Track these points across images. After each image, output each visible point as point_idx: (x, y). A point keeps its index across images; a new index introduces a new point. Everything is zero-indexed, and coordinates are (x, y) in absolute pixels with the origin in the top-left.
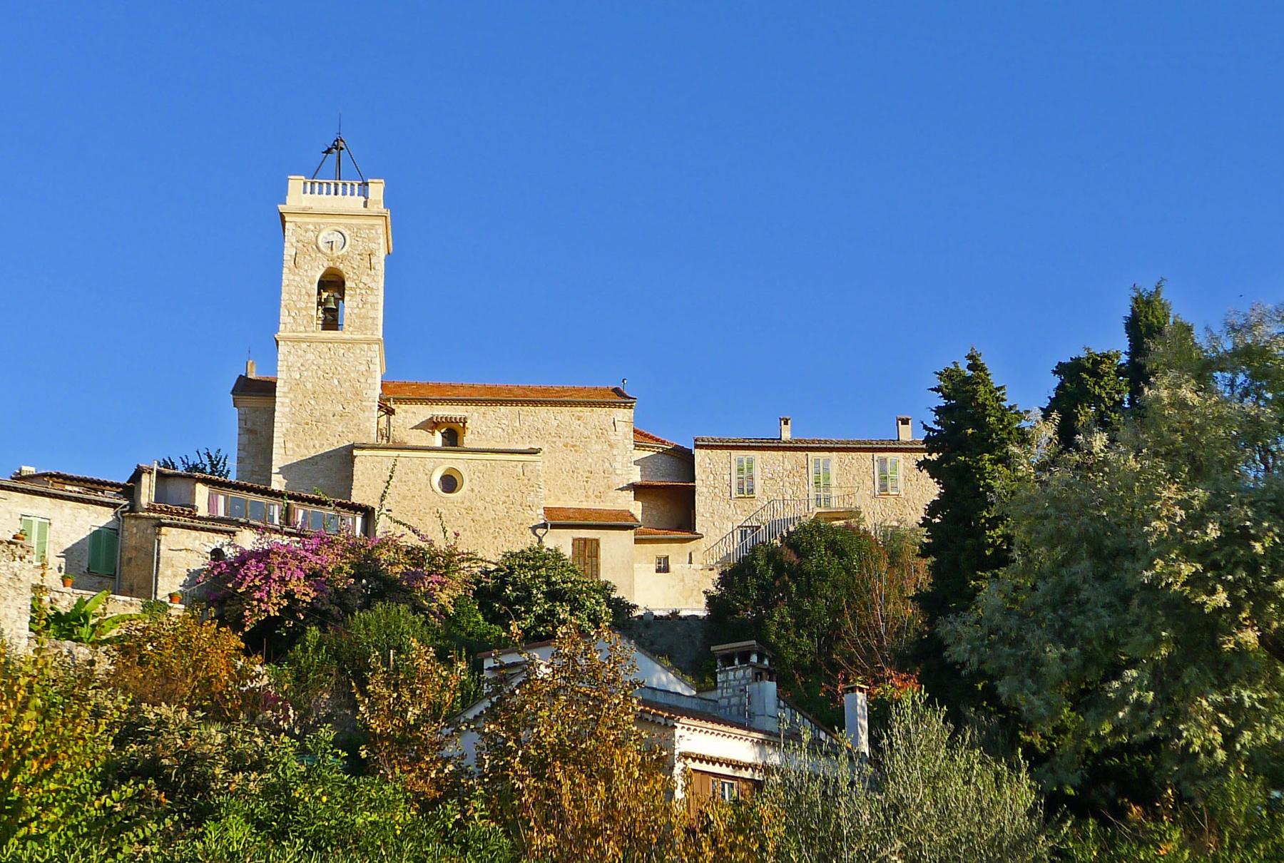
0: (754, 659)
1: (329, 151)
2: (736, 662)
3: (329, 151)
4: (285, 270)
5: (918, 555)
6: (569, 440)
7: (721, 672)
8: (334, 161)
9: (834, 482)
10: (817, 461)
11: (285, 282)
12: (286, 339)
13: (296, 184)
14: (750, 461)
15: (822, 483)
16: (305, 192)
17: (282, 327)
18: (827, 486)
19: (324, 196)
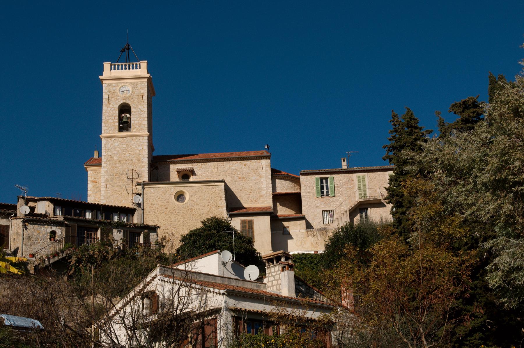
0: (283, 260)
1: (123, 51)
2: (275, 262)
3: (123, 51)
4: (104, 106)
5: (159, 227)
6: (240, 176)
7: (268, 268)
8: (125, 56)
9: (367, 187)
10: (359, 177)
11: (104, 111)
12: (105, 137)
13: (107, 66)
14: (364, 177)
15: (362, 188)
16: (111, 69)
17: (103, 132)
18: (365, 188)
19: (131, 70)
